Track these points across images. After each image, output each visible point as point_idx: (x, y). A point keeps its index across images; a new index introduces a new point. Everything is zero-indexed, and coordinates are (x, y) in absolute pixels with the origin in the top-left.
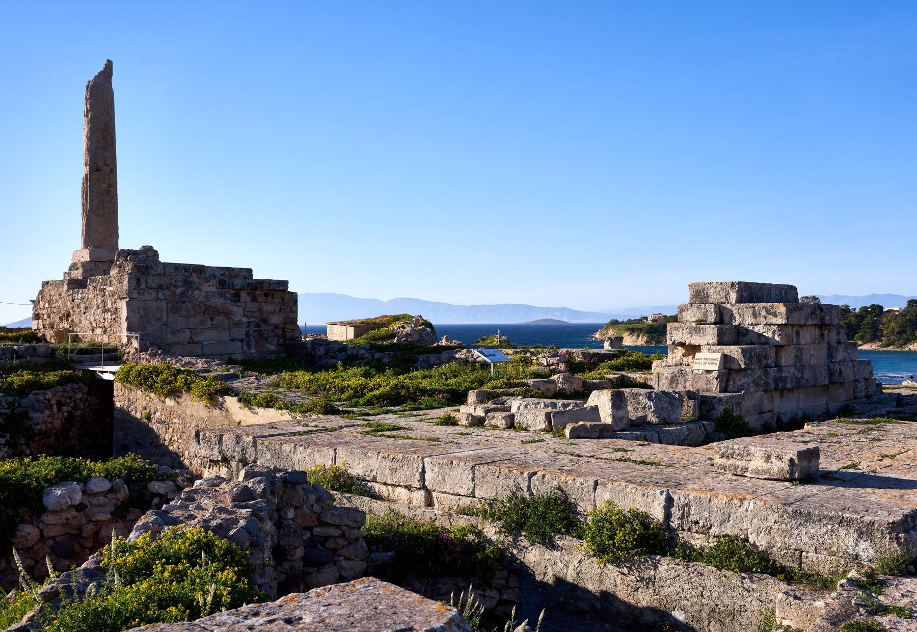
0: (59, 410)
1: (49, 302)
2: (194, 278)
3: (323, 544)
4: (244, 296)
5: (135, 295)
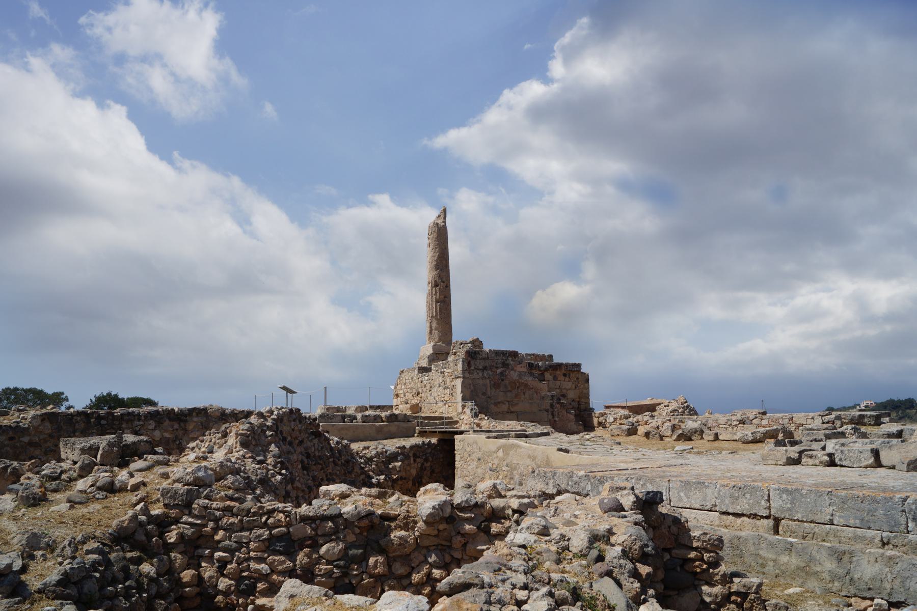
0: (415, 461)
1: (405, 384)
2: (510, 361)
3: (682, 566)
4: (547, 375)
5: (467, 375)
